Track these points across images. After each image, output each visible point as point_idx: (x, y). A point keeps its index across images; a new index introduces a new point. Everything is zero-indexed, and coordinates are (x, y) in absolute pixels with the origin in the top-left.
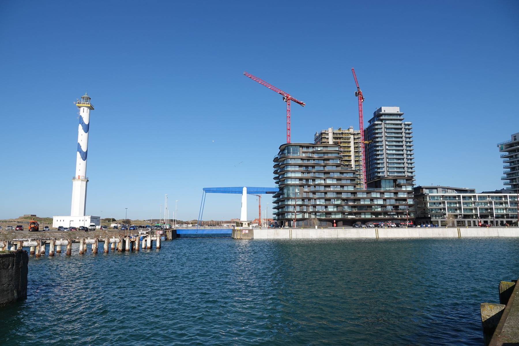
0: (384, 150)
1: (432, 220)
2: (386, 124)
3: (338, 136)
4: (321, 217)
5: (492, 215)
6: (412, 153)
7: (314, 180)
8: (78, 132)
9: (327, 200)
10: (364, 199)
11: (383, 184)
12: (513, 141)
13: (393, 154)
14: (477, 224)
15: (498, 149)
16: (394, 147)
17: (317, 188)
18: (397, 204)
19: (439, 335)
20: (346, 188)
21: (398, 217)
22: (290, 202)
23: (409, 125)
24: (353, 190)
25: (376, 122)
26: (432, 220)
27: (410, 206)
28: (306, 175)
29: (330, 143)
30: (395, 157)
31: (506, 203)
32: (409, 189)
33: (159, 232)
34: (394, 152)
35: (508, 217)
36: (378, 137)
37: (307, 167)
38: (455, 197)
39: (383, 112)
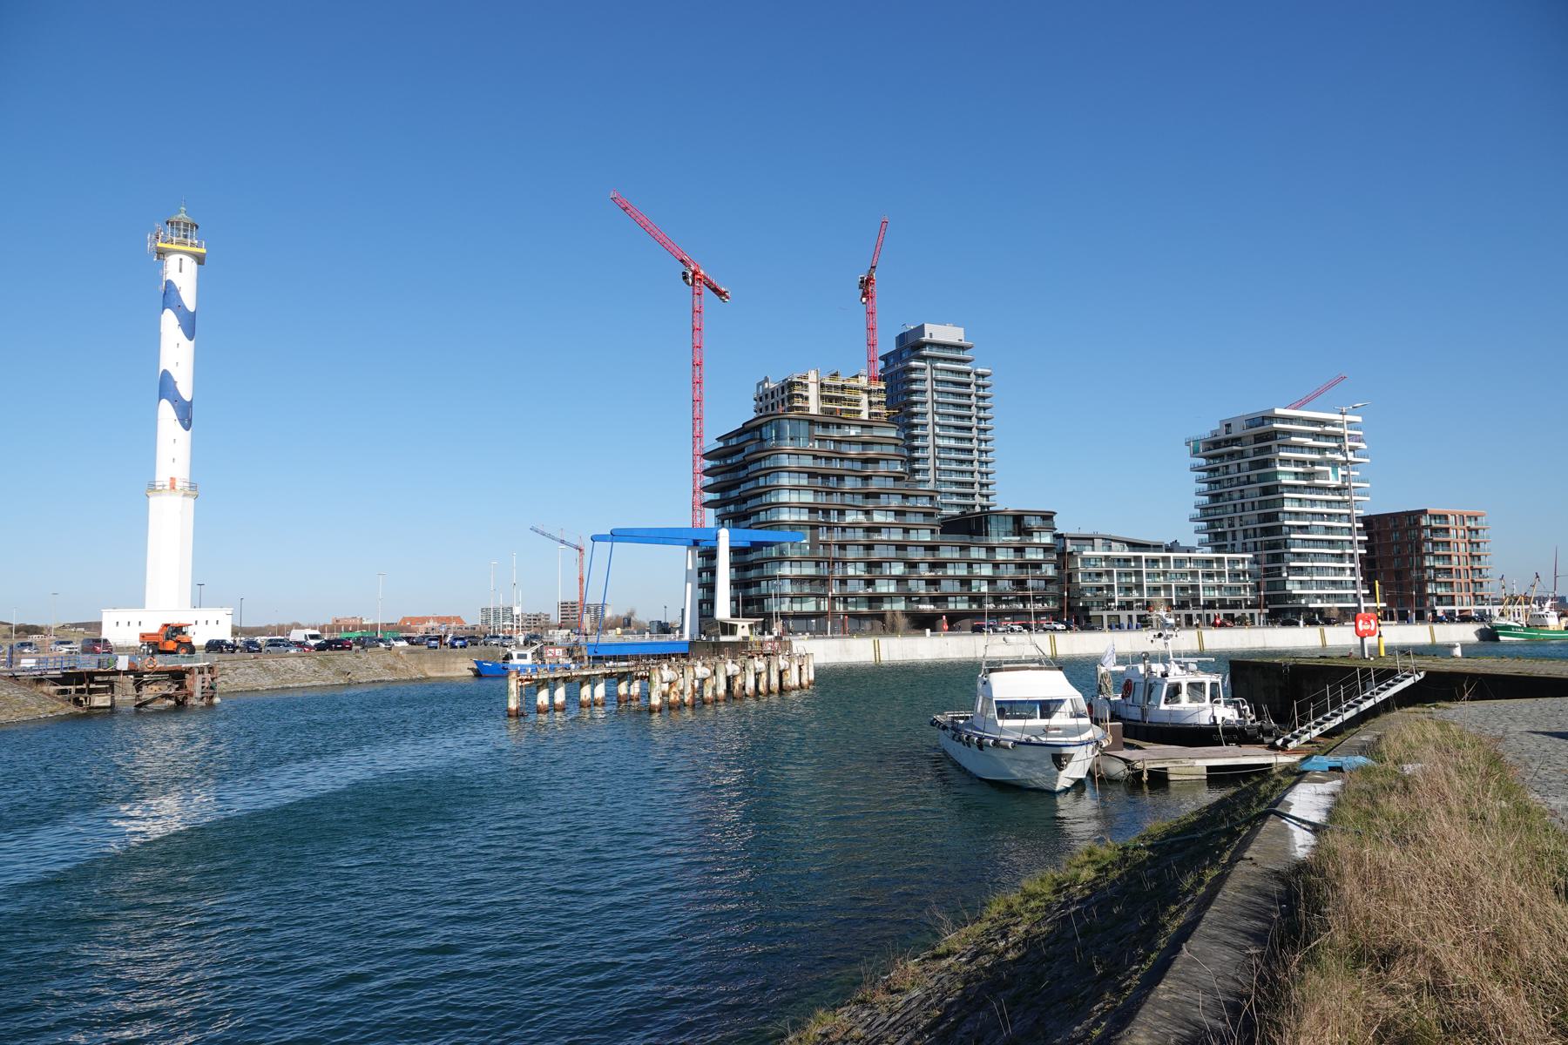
0: (931, 438)
1: (1091, 613)
2: (936, 369)
3: (833, 394)
4: (859, 609)
5: (1196, 601)
6: (988, 448)
7: (841, 513)
8: (160, 334)
9: (871, 565)
10: (954, 562)
11: (992, 528)
12: (1223, 436)
13: (950, 449)
14: (1212, 620)
15: (1188, 450)
16: (952, 429)
17: (849, 535)
18: (1023, 577)
19: (396, 1002)
20: (913, 536)
21: (1024, 606)
22: (786, 570)
23: (983, 376)
24: (929, 539)
25: (914, 364)
26: (1091, 613)
27: (1048, 581)
28: (822, 499)
29: (810, 412)
30: (953, 455)
31: (1221, 574)
32: (1047, 539)
33: (552, 650)
34: (952, 443)
35: (1223, 606)
36: (916, 403)
37: (825, 477)
38: (1127, 560)
39: (926, 338)
